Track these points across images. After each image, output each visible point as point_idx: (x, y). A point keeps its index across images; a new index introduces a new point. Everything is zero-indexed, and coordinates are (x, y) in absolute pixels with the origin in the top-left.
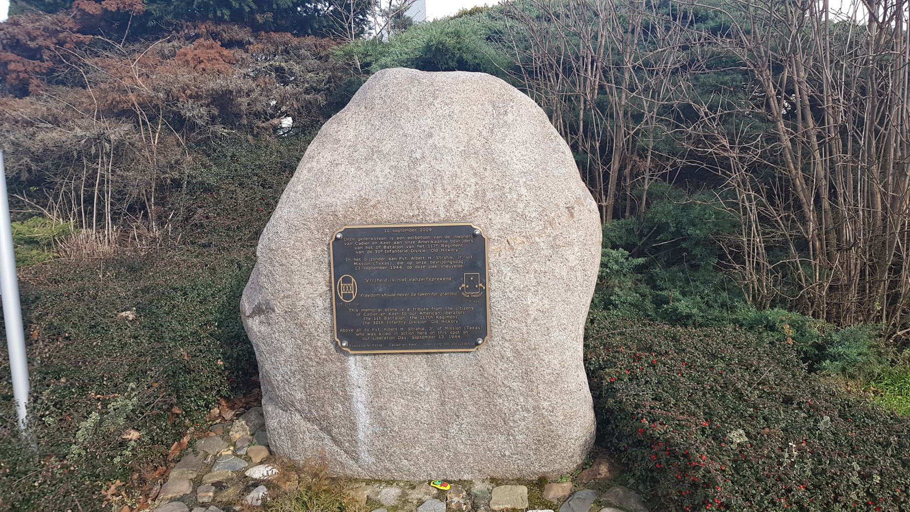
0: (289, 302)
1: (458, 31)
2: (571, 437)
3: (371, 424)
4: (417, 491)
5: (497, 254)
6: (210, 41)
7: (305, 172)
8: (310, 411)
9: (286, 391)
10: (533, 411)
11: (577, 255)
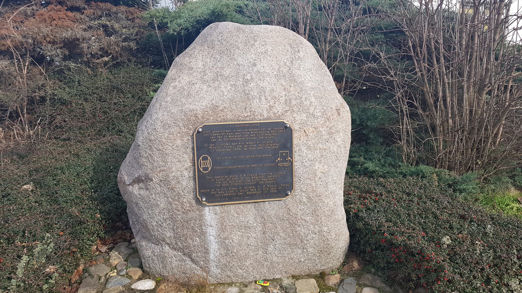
0: (164, 174)
1: (228, 5)
2: (339, 247)
3: (219, 249)
4: (249, 288)
5: (299, 139)
6: (59, 7)
7: (171, 89)
8: (176, 243)
9: (159, 231)
10: (318, 234)
11: (342, 138)
